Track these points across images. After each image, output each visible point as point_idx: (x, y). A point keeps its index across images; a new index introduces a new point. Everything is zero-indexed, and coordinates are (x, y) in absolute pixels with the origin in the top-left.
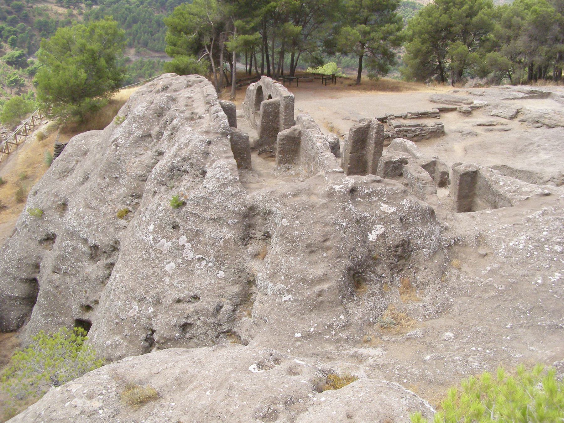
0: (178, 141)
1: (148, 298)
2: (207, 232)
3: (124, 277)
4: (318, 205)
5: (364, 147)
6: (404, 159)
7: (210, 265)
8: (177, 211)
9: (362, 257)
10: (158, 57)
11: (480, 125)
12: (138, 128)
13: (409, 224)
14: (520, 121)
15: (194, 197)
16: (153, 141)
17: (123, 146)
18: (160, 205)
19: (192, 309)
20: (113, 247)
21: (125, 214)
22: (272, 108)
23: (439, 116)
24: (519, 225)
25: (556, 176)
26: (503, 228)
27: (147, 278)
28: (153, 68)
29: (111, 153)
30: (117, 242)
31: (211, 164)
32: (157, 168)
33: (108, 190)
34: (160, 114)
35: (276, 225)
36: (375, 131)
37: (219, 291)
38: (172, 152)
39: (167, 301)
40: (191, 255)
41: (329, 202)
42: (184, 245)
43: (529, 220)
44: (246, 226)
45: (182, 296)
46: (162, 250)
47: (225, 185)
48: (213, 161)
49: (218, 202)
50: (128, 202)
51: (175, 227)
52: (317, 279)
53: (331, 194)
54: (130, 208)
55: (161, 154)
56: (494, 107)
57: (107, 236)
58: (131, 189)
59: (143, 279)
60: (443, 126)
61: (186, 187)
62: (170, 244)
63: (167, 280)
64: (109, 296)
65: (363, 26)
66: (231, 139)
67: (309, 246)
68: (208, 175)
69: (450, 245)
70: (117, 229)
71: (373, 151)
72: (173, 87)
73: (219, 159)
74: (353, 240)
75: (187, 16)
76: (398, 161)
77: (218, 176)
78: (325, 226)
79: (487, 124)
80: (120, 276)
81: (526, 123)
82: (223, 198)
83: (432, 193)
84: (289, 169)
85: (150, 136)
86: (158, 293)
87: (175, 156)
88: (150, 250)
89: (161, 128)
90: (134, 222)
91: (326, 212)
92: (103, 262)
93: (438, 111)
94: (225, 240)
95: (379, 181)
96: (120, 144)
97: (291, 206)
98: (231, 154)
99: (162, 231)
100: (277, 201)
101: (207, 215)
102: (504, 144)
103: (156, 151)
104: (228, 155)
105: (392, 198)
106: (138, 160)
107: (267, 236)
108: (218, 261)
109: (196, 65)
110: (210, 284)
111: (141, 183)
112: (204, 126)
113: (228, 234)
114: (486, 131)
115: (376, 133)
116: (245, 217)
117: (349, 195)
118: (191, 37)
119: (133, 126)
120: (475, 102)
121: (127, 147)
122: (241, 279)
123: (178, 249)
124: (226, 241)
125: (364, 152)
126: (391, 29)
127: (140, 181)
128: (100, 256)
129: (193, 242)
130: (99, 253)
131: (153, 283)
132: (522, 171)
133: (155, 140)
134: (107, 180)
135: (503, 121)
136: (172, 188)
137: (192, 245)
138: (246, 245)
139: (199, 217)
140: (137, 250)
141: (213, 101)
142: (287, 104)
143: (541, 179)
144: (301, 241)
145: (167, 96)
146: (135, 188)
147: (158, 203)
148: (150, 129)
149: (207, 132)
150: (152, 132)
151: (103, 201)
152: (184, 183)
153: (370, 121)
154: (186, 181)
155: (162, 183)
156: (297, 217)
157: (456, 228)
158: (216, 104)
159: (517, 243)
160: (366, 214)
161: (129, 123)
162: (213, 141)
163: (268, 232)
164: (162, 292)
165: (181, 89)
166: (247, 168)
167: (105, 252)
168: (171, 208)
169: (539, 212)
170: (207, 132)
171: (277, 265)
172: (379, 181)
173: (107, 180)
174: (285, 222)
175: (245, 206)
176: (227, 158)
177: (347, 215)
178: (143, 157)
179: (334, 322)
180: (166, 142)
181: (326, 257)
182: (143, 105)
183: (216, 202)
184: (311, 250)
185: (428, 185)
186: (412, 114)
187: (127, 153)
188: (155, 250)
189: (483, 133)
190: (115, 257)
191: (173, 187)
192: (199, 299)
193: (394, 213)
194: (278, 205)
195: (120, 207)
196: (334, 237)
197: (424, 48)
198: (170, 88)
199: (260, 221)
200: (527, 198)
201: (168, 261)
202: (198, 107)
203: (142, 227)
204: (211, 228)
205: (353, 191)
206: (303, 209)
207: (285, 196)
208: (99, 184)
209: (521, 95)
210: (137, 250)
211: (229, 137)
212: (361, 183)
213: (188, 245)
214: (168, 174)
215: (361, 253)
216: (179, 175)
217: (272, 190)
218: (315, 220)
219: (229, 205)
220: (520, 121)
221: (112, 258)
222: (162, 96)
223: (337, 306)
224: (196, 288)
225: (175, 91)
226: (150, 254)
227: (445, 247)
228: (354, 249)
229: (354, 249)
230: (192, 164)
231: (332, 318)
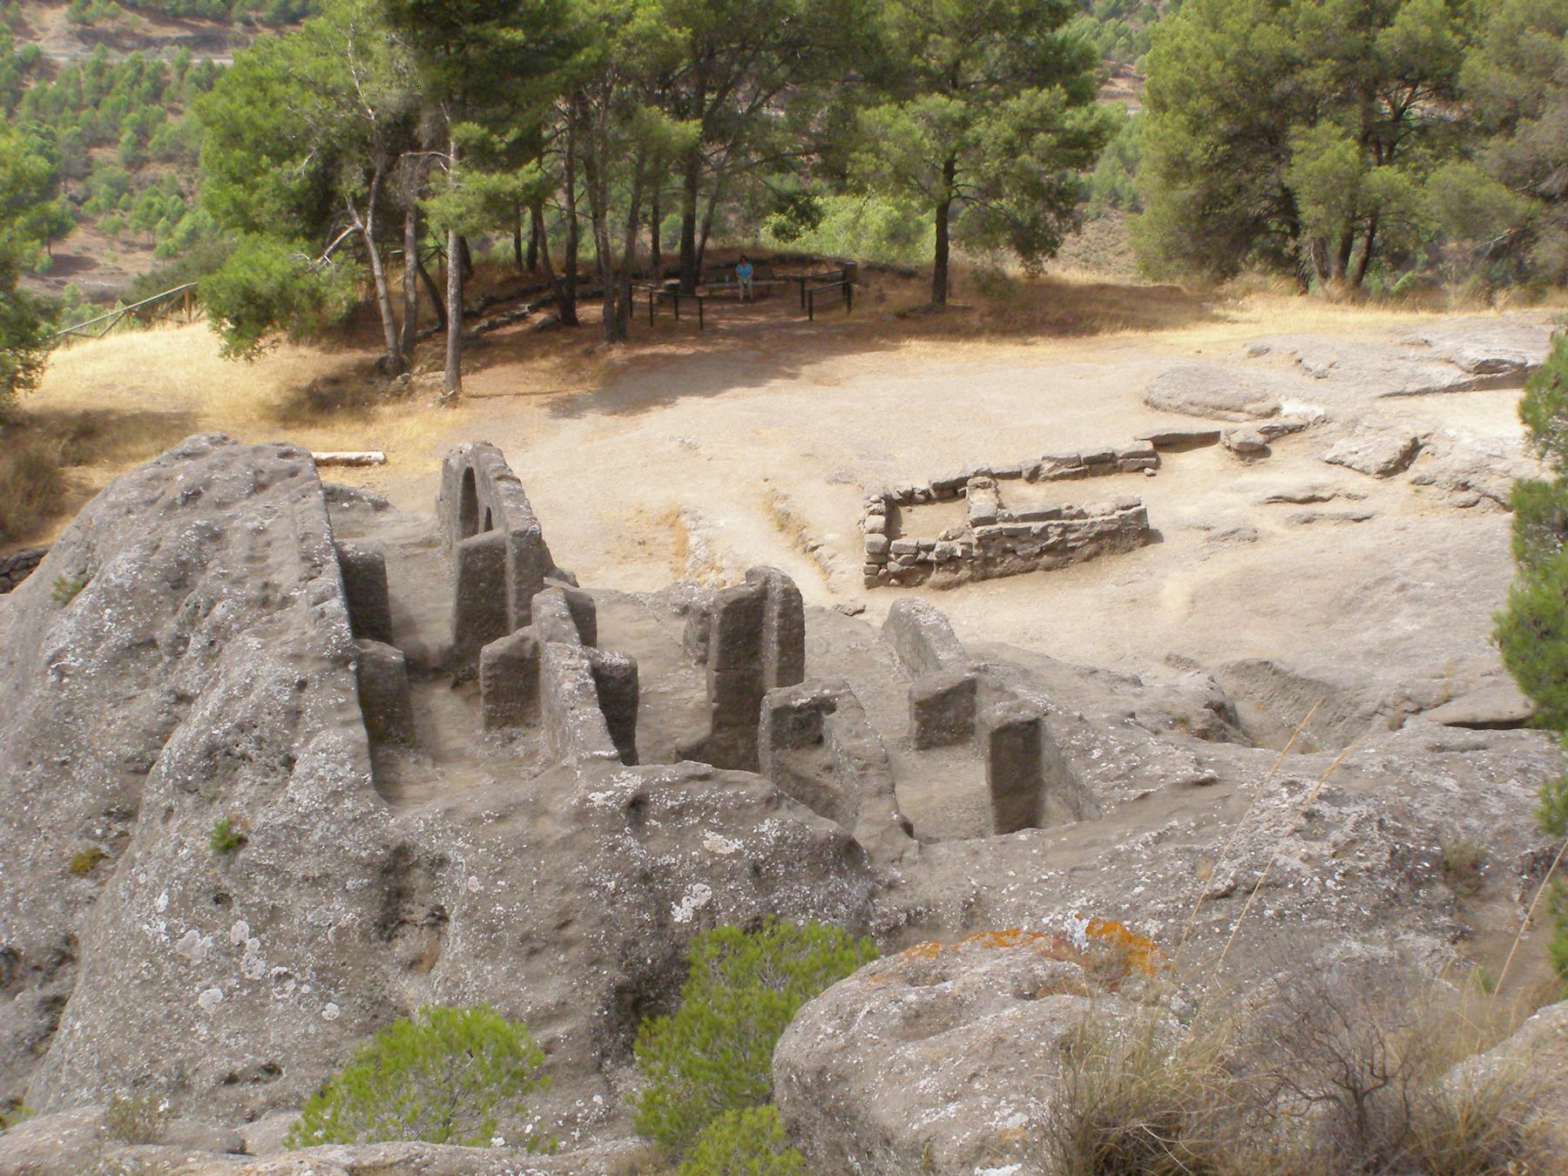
0: (225, 676)
1: (156, 1076)
2: (297, 910)
3: (95, 1028)
4: (551, 842)
5: (756, 653)
6: (826, 699)
7: (306, 989)
8: (224, 859)
9: (654, 961)
10: (178, 42)
11: (1278, 499)
12: (117, 621)
13: (774, 878)
14: (1413, 483)
15: (265, 824)
16: (161, 658)
17: (79, 673)
18: (181, 844)
19: (262, 1098)
20: (60, 952)
21: (89, 865)
22: (484, 560)
23: (1156, 466)
24: (1086, 869)
25: (1390, 700)
26: (1040, 880)
27: (153, 1028)
28: (156, 94)
29: (46, 693)
30: (70, 940)
31: (307, 742)
32: (171, 751)
33: (43, 797)
34: (179, 580)
35: (456, 889)
36: (777, 609)
37: (327, 1052)
38: (210, 707)
39: (203, 1082)
40: (260, 966)
41: (578, 832)
42: (242, 945)
43: (1114, 857)
44: (389, 894)
45: (239, 1066)
46: (188, 956)
47: (337, 795)
48: (311, 734)
49: (322, 838)
50: (99, 832)
51: (221, 899)
52: (543, 1013)
53: (582, 814)
54: (104, 848)
55: (183, 699)
56: (1345, 425)
57: (44, 925)
58: (104, 794)
59: (142, 1030)
60: (1142, 515)
61: (245, 800)
62: (208, 941)
63: (202, 1030)
64: (56, 1080)
65: (938, 99)
66: (358, 672)
67: (526, 938)
68: (299, 769)
69: (896, 927)
70: (71, 905)
71: (775, 666)
72: (214, 493)
73: (325, 728)
74: (632, 921)
75: (278, 89)
76: (808, 706)
77: (321, 772)
78: (563, 892)
79: (1300, 496)
80: (84, 1028)
81: (1432, 489)
82: (333, 828)
83: (880, 793)
84: (512, 740)
85: (152, 643)
86: (181, 1062)
87: (217, 718)
88: (160, 959)
89: (181, 625)
90: (117, 886)
91: (567, 857)
92: (31, 994)
93: (1149, 446)
94: (340, 929)
95: (705, 778)
96: (70, 668)
97: (490, 844)
98: (357, 712)
99: (189, 909)
100: (457, 833)
101: (298, 869)
102: (1316, 577)
103: (171, 692)
104: (348, 716)
105: (733, 819)
106: (121, 714)
107: (439, 918)
108: (323, 980)
109: (312, 279)
110: (306, 1035)
111: (131, 779)
112: (291, 635)
113: (344, 912)
114: (1291, 522)
115: (781, 616)
116: (386, 871)
117: (628, 814)
118: (296, 171)
119: (106, 617)
120: (1287, 408)
121: (89, 678)
122: (378, 1021)
123: (228, 955)
124: (342, 932)
125: (756, 666)
126: (1041, 110)
127: (128, 772)
128: (23, 978)
129: (263, 936)
130: (19, 969)
131: (168, 1039)
132: (1309, 682)
133: (167, 659)
134: (38, 768)
135: (1356, 483)
136: (211, 800)
137: (263, 943)
138: (389, 939)
139: (277, 874)
140: (126, 959)
141: (320, 552)
142: (521, 552)
143: (1357, 706)
144: (508, 927)
145: (198, 528)
146: (115, 793)
147: (176, 841)
148: (151, 626)
149: (297, 658)
150: (157, 634)
151: (28, 828)
152: (240, 788)
153: (767, 581)
154: (246, 783)
155: (185, 788)
156: (501, 872)
157: (920, 884)
158: (328, 562)
159: (1060, 917)
160: (668, 859)
161: (94, 608)
162: (313, 680)
163: (441, 908)
164: (191, 1060)
165: (236, 501)
166: (403, 741)
167: (37, 968)
168: (210, 853)
169: (1148, 835)
170: (297, 658)
171: (456, 985)
172: (705, 778)
173: (38, 768)
174: (474, 883)
175: (386, 847)
176: (346, 724)
177: (619, 864)
178: (136, 708)
179: (580, 1109)
180: (196, 669)
181: (565, 963)
182: (130, 555)
183: (316, 838)
184: (531, 948)
185: (871, 771)
186: (1060, 462)
187: (90, 696)
188: (173, 958)
189: (1280, 530)
190: (67, 980)
191: (214, 798)
192: (280, 1073)
193: (738, 854)
194: (460, 843)
195: (77, 846)
196: (585, 915)
197: (1198, 151)
198: (206, 496)
199: (421, 881)
200: (1144, 796)
201: (205, 982)
202: (281, 564)
203: (138, 899)
204: (306, 901)
205: (637, 805)
206: (515, 853)
207: (476, 820)
208: (15, 781)
209: (1452, 375)
210: (126, 959)
211: (352, 667)
212: (659, 784)
213: (253, 944)
214: (202, 764)
215: (649, 953)
216: (229, 767)
217: (448, 805)
218: (543, 875)
219: (347, 845)
220: (1413, 483)
221: (56, 983)
222: (182, 528)
223: (587, 1074)
224: (273, 1047)
225: (221, 505)
226: (159, 968)
227: (879, 932)
228: (635, 943)
229: (635, 943)
230: (260, 740)
231: (574, 1101)
